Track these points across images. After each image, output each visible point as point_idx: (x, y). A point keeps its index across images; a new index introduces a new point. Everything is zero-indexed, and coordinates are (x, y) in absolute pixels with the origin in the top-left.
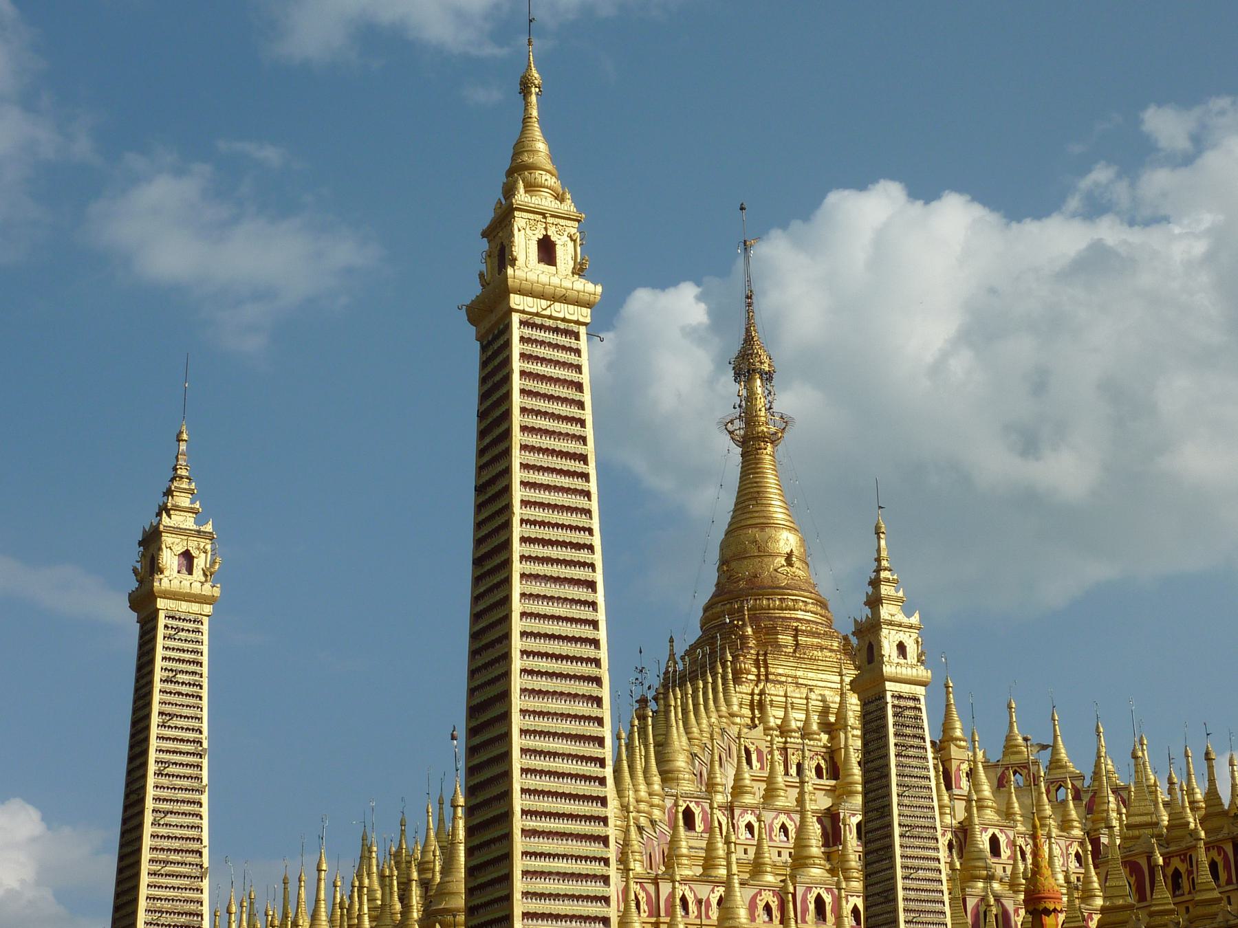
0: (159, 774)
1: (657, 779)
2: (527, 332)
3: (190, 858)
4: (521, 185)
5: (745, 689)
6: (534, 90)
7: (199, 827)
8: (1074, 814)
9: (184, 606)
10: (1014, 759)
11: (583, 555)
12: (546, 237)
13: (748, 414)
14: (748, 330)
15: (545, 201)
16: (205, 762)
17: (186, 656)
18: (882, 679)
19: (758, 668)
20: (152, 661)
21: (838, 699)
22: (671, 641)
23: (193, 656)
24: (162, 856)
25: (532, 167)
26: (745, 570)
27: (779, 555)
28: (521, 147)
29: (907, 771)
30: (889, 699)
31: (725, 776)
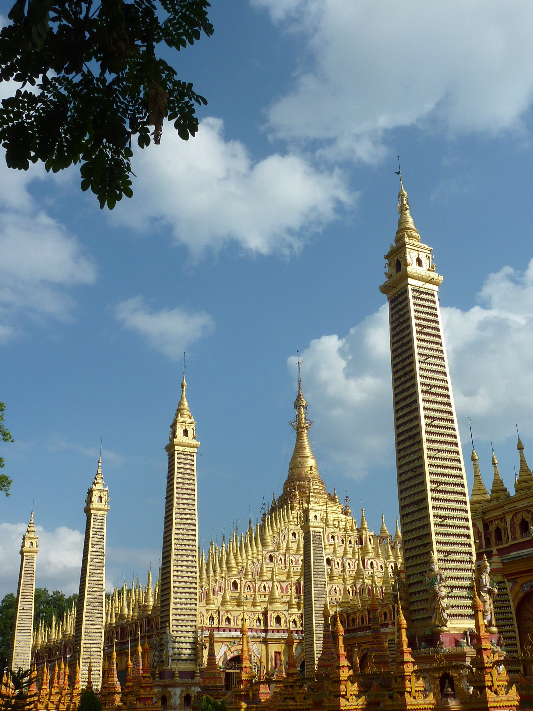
0: (91, 562)
1: (260, 546)
2: (180, 456)
3: (100, 586)
4: (179, 415)
6: (185, 387)
7: (103, 577)
8: (399, 554)
10: (383, 535)
11: (192, 517)
12: (186, 429)
13: (299, 420)
14: (299, 392)
15: (186, 419)
16: (104, 558)
17: (100, 527)
18: (309, 527)
19: (300, 505)
20: (90, 529)
21: (325, 515)
22: (274, 494)
23: (102, 527)
24: (92, 586)
26: (296, 472)
27: (308, 467)
28: (180, 404)
29: (316, 554)
30: (311, 533)
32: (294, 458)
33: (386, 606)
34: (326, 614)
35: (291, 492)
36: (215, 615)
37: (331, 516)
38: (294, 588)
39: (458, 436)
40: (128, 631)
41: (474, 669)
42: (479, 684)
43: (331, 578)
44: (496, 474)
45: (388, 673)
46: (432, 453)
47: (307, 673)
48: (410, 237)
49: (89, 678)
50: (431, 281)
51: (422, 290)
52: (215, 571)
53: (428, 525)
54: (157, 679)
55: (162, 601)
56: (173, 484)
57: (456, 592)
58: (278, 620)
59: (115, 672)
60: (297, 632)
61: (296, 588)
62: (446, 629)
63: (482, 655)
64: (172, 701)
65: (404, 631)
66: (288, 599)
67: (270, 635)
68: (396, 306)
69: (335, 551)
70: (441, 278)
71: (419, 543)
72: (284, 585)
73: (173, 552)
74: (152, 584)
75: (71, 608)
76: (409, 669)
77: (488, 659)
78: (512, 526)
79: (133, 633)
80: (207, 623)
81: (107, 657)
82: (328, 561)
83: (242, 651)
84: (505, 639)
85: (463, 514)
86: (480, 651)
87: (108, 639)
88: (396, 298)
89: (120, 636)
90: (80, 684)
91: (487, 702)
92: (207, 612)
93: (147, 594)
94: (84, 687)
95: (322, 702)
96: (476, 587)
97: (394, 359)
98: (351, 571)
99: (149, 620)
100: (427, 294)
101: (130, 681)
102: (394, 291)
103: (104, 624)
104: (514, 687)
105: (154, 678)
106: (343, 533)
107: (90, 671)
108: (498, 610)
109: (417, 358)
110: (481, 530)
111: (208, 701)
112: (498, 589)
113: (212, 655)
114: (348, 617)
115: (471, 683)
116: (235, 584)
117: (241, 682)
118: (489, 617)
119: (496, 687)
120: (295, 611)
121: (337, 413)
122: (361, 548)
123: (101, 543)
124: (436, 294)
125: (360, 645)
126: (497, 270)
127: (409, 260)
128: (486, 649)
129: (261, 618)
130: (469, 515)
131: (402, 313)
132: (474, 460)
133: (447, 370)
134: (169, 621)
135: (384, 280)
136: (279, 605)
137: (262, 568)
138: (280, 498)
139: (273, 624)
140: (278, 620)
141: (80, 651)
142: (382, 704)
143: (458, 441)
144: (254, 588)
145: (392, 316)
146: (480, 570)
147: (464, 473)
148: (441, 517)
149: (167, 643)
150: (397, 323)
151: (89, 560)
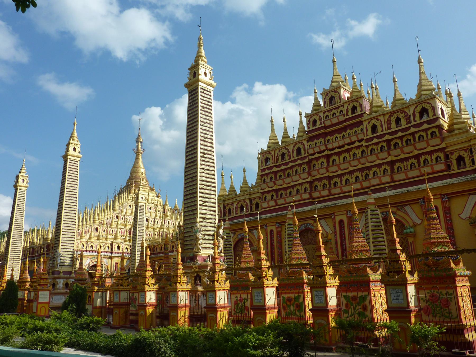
1: (112, 211)
5: (132, 195)
9: (22, 188)
15: (75, 142)
25: (73, 137)
26: (134, 175)
28: (72, 133)
31: (124, 211)
32: (133, 168)
33: (174, 242)
34: (142, 246)
35: (130, 185)
36: (85, 244)
37: (150, 198)
38: (128, 232)
39: (215, 163)
40: (36, 250)
41: (211, 273)
42: (212, 280)
43: (148, 228)
44: (232, 183)
45: (170, 274)
46: (202, 170)
47: (131, 273)
48: (202, 60)
49: (12, 274)
50: (210, 85)
51: (206, 89)
52: (86, 222)
53: (196, 205)
54: (51, 275)
55: (56, 236)
56: (65, 176)
57: (207, 237)
58: (118, 247)
59: (27, 271)
60: (128, 253)
61: (129, 232)
62: (200, 254)
63: (215, 266)
64: (58, 286)
65: (180, 254)
66: (124, 238)
67: (113, 255)
68: (192, 95)
69: (151, 215)
70: (215, 84)
71: (191, 213)
72: (123, 230)
73: (63, 211)
74: (51, 227)
75: (4, 238)
76: (180, 272)
77: (218, 268)
78: (236, 208)
79: (39, 252)
80: (80, 248)
81: (23, 263)
82: (147, 220)
83: (97, 262)
84: (227, 259)
85: (213, 201)
86: (214, 264)
87: (24, 255)
88: (192, 91)
89: (31, 253)
90: (7, 277)
91: (215, 288)
92: (81, 242)
93: (48, 232)
94: (138, 62)
95: (137, 287)
96: (217, 235)
97: (188, 122)
98: (158, 225)
99: (48, 245)
100: (208, 91)
101: (35, 276)
102: (191, 87)
103: (22, 246)
104: (228, 281)
105: (49, 274)
106: (156, 206)
107: (12, 270)
108: (226, 246)
109: (200, 123)
110: (222, 209)
111: (77, 286)
112: (226, 236)
113: (81, 263)
114: (153, 248)
115: (208, 279)
116: (97, 229)
117: (95, 277)
118: (221, 249)
119: (220, 281)
120: (128, 243)
121: (156, 147)
122: (164, 214)
123: (22, 203)
124: (212, 92)
125: (159, 261)
126: (240, 85)
127: (200, 73)
128: (217, 264)
129: (110, 246)
130: (216, 201)
131: (194, 99)
132: (222, 175)
133: (213, 131)
134: (59, 246)
135: (187, 81)
136: (119, 240)
137: (112, 222)
138: (124, 187)
139: (115, 249)
140: (118, 247)
141: (7, 260)
142: (166, 288)
143: (215, 165)
144: (107, 231)
145: (189, 100)
146: (219, 227)
147: (216, 181)
148: (203, 201)
149: (57, 257)
150: (192, 104)
151: (15, 213)
